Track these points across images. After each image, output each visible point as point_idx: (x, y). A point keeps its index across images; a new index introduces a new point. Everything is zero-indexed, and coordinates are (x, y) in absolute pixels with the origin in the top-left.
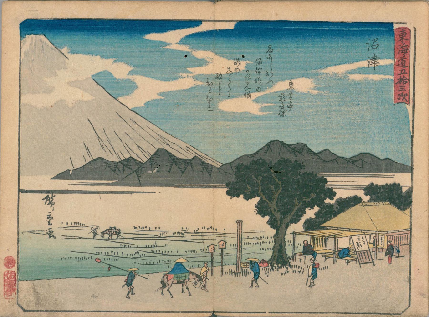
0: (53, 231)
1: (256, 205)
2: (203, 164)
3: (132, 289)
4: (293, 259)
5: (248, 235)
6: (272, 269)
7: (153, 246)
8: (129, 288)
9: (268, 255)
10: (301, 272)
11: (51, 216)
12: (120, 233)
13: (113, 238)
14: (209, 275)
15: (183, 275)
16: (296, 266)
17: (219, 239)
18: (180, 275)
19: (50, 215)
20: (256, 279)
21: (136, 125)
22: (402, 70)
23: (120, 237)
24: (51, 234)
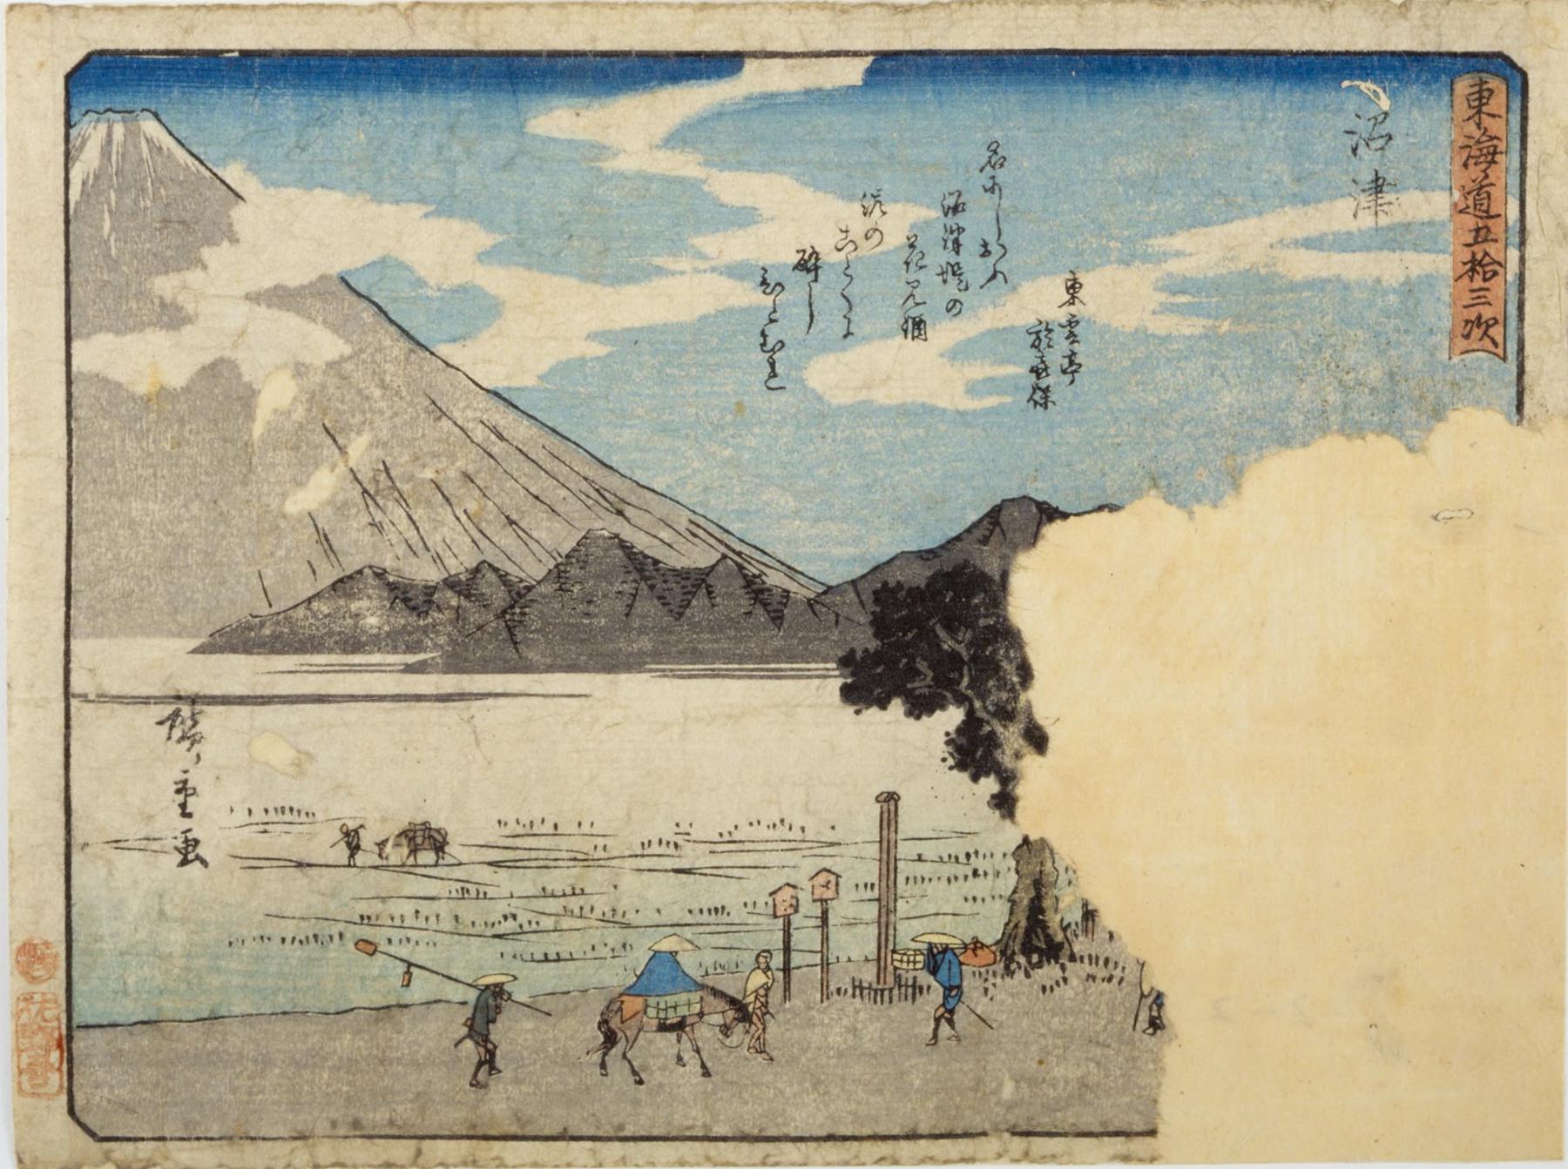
0: (197, 842)
1: (947, 734)
2: (755, 589)
3: (492, 1054)
4: (1086, 931)
5: (921, 847)
6: (1009, 972)
7: (568, 891)
8: (482, 1050)
9: (991, 924)
10: (366, 932)
11: (189, 785)
12: (445, 843)
13: (420, 862)
14: (776, 996)
15: (684, 997)
16: (1094, 960)
17: (810, 866)
18: (671, 1000)
19: (185, 782)
20: (947, 1015)
21: (503, 444)
22: (1478, 230)
23: (449, 860)
24: (189, 852)
